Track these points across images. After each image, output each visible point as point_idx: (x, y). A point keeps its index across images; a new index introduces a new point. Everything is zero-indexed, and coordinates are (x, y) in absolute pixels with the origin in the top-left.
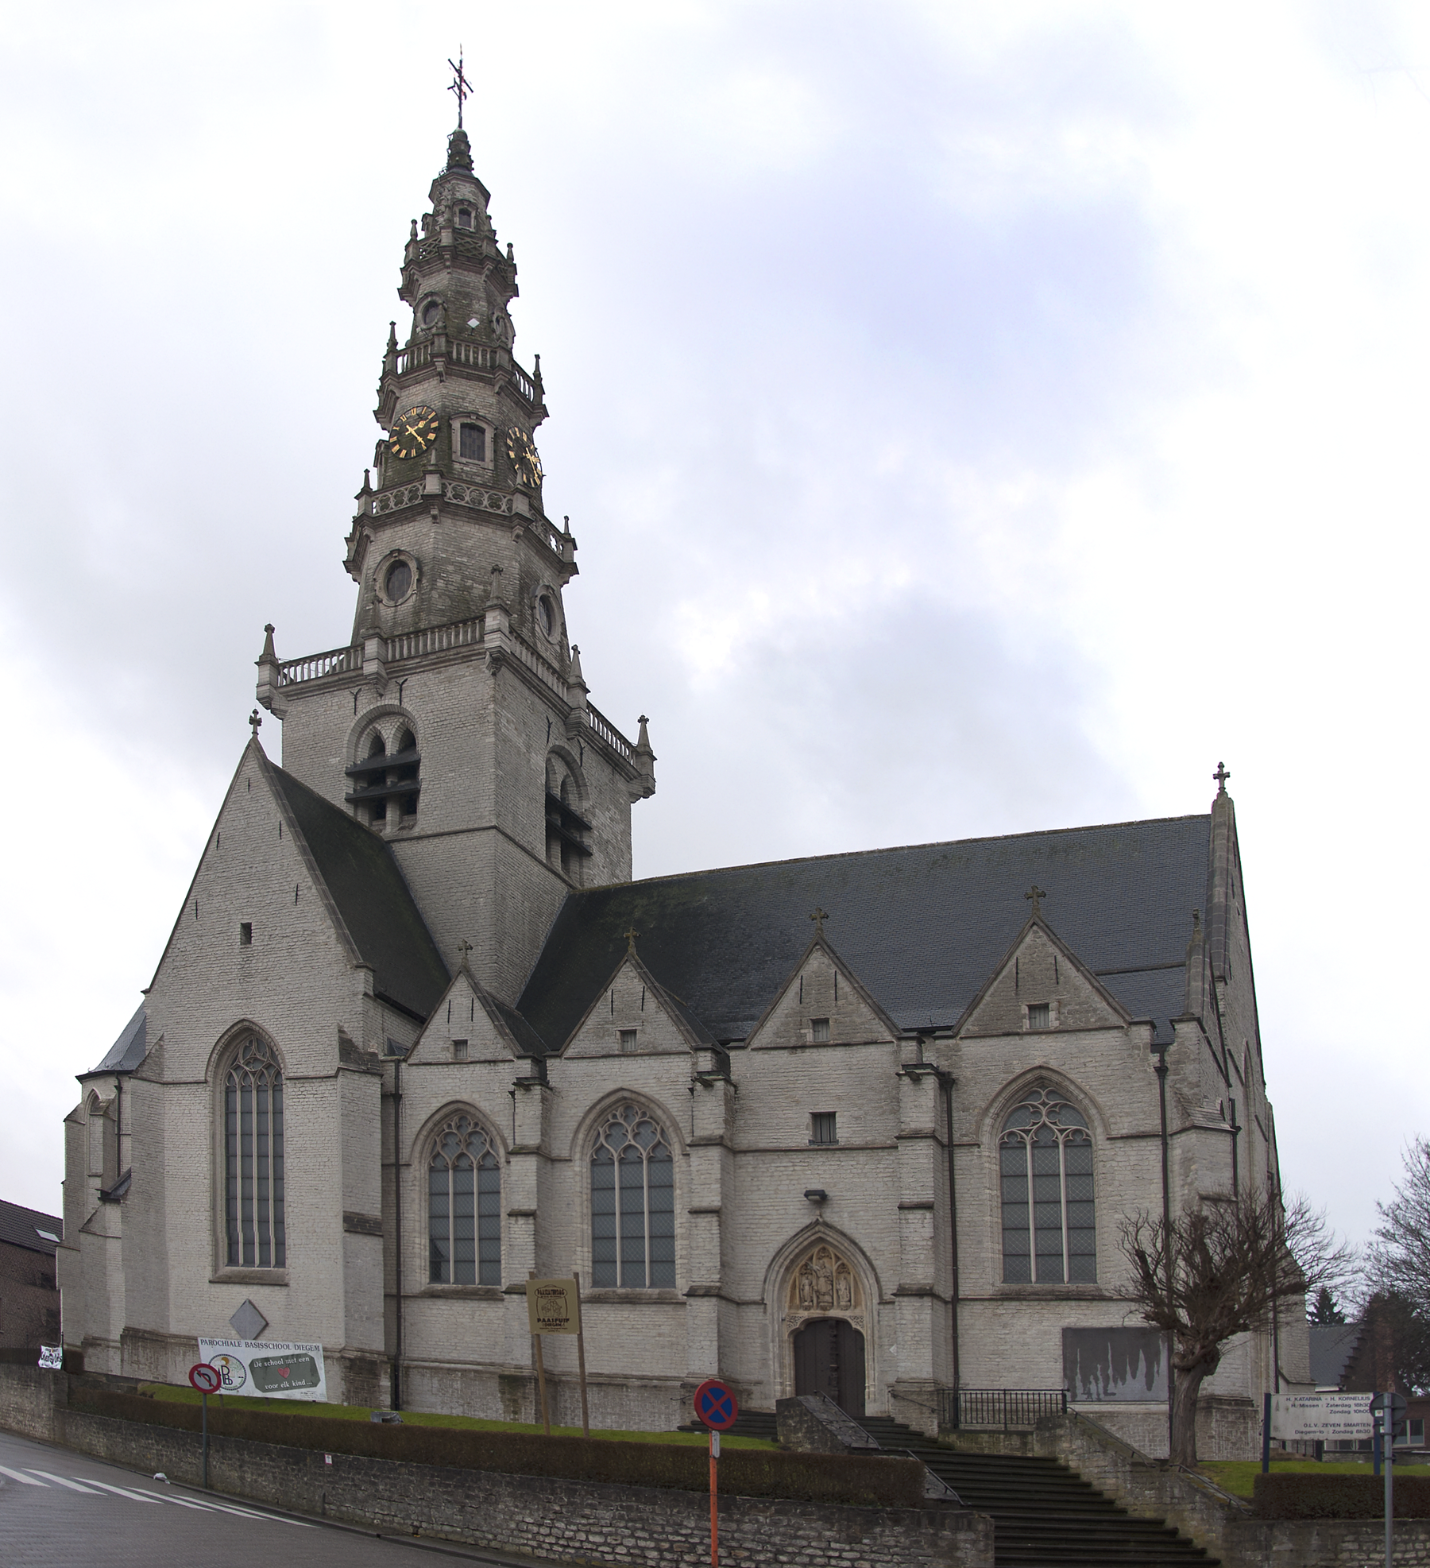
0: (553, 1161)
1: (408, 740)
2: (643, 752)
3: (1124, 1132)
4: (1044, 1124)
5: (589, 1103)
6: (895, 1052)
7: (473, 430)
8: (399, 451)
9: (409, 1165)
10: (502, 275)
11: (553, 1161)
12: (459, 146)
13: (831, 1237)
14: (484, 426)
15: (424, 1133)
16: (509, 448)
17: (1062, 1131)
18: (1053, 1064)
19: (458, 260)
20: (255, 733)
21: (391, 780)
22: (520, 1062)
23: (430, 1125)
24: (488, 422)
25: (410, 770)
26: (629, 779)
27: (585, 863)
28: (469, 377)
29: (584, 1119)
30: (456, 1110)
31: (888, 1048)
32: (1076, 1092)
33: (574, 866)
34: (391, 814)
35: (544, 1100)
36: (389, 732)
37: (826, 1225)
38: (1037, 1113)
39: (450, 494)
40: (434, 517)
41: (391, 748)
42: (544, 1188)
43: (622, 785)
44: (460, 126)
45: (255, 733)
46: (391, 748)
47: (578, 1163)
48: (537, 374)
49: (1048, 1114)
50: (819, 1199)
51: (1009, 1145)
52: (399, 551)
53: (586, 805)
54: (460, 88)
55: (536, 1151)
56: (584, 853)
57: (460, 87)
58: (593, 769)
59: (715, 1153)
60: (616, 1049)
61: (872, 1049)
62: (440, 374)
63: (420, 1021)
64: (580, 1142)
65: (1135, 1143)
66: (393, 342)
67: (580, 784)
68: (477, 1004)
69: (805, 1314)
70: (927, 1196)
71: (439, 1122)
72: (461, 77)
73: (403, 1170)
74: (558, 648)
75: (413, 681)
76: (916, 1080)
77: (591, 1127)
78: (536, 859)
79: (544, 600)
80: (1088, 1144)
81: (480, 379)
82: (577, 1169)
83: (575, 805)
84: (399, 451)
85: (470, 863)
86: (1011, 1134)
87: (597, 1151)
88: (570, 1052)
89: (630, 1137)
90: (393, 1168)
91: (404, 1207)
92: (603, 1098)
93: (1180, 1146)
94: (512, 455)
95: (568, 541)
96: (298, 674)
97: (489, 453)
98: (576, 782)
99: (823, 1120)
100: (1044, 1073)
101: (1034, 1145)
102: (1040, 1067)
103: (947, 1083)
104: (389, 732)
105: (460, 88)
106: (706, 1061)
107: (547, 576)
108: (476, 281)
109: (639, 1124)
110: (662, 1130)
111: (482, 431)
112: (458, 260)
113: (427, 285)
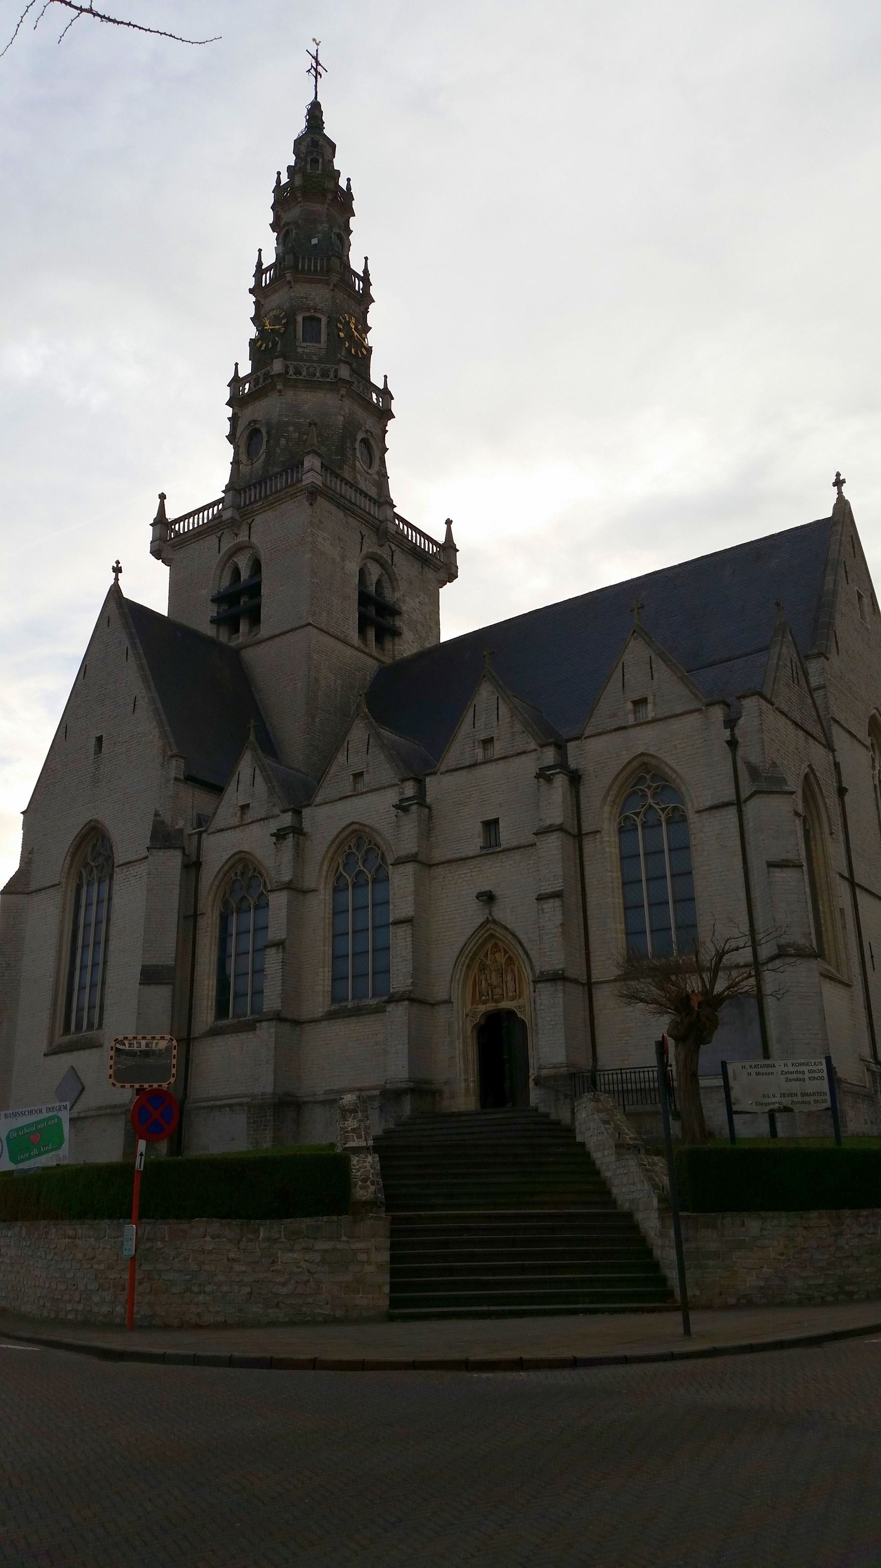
0: (305, 892)
1: (256, 566)
2: (449, 547)
3: (708, 804)
4: (650, 806)
5: (331, 838)
6: (539, 759)
7: (312, 321)
8: (261, 345)
9: (203, 914)
10: (343, 202)
11: (305, 892)
12: (315, 113)
13: (499, 932)
14: (319, 315)
15: (216, 883)
16: (340, 330)
17: (663, 810)
18: (652, 751)
19: (313, 200)
20: (117, 579)
21: (240, 602)
22: (284, 815)
23: (221, 875)
24: (322, 312)
25: (255, 590)
26: (437, 569)
27: (396, 640)
28: (310, 282)
29: (327, 852)
30: (240, 859)
31: (533, 756)
32: (670, 773)
33: (388, 645)
34: (243, 627)
35: (297, 845)
36: (243, 563)
37: (495, 922)
38: (645, 796)
39: (291, 372)
40: (280, 391)
41: (245, 575)
42: (294, 920)
43: (430, 575)
44: (316, 98)
45: (117, 579)
46: (245, 575)
47: (322, 891)
48: (366, 271)
49: (654, 795)
50: (488, 898)
51: (625, 829)
52: (255, 421)
53: (397, 595)
54: (316, 70)
55: (288, 886)
56: (396, 633)
57: (316, 71)
58: (404, 567)
59: (410, 868)
60: (348, 790)
61: (523, 758)
62: (289, 282)
63: (218, 790)
64: (324, 873)
65: (717, 813)
66: (259, 264)
67: (392, 579)
68: (257, 771)
69: (482, 1008)
70: (557, 886)
71: (228, 872)
72: (318, 63)
73: (199, 918)
74: (376, 477)
75: (259, 519)
76: (549, 780)
77: (332, 859)
78: (353, 646)
79: (365, 441)
80: (684, 819)
81: (319, 281)
82: (322, 897)
83: (390, 596)
84: (261, 345)
85: (303, 654)
86: (627, 817)
87: (337, 880)
88: (318, 799)
89: (360, 863)
90: (190, 918)
91: (198, 951)
92: (340, 833)
93: (750, 809)
94: (342, 335)
95: (386, 394)
96: (181, 527)
97: (324, 337)
98: (390, 578)
99: (491, 826)
100: (645, 759)
101: (644, 826)
102: (642, 754)
103: (575, 779)
104: (375, 572)
105: (316, 70)
106: (410, 789)
107: (370, 423)
108: (320, 208)
109: (368, 851)
110: (383, 854)
111: (319, 320)
112: (313, 200)
113: (286, 218)
